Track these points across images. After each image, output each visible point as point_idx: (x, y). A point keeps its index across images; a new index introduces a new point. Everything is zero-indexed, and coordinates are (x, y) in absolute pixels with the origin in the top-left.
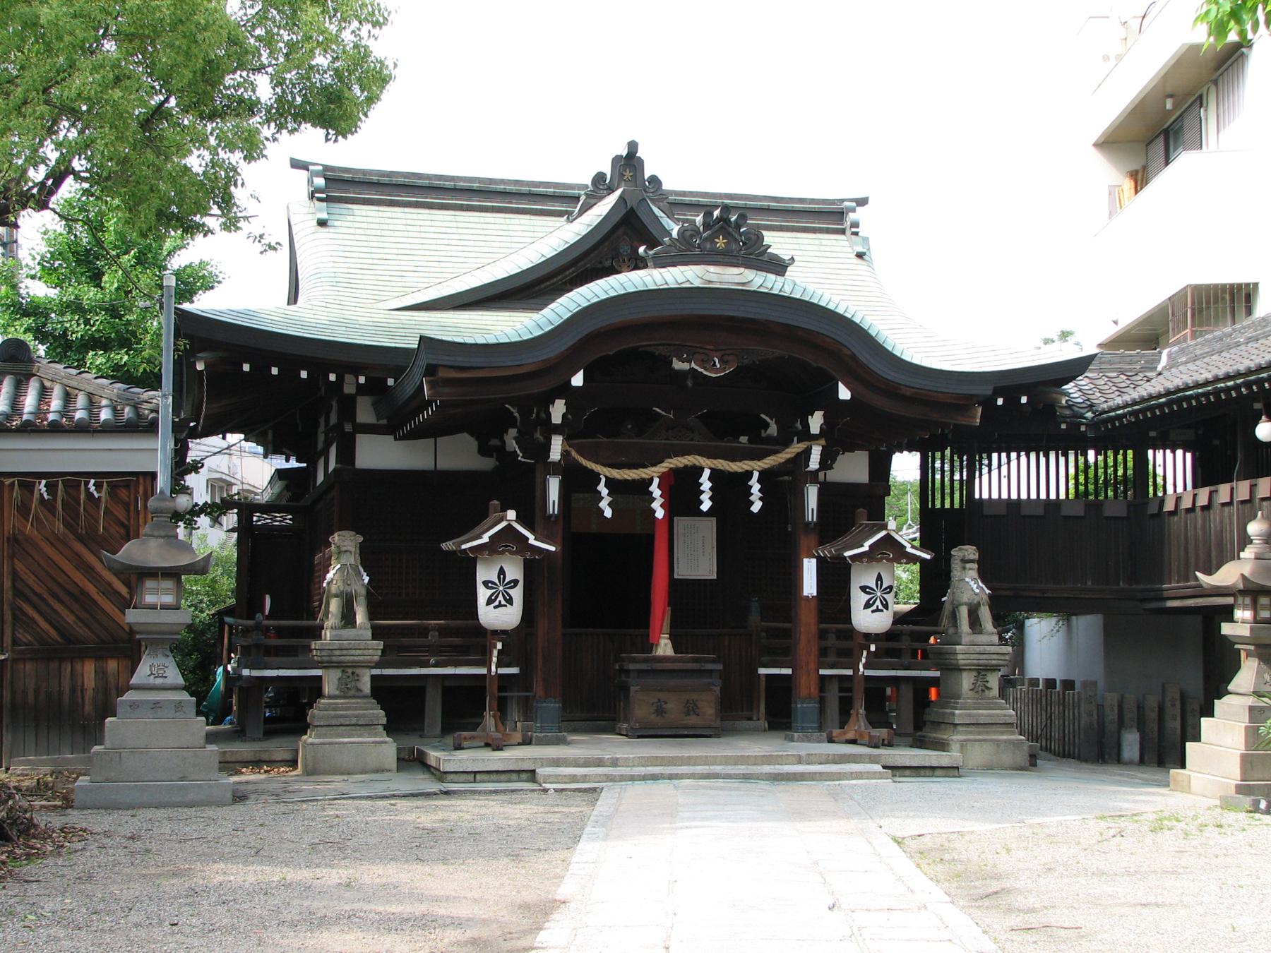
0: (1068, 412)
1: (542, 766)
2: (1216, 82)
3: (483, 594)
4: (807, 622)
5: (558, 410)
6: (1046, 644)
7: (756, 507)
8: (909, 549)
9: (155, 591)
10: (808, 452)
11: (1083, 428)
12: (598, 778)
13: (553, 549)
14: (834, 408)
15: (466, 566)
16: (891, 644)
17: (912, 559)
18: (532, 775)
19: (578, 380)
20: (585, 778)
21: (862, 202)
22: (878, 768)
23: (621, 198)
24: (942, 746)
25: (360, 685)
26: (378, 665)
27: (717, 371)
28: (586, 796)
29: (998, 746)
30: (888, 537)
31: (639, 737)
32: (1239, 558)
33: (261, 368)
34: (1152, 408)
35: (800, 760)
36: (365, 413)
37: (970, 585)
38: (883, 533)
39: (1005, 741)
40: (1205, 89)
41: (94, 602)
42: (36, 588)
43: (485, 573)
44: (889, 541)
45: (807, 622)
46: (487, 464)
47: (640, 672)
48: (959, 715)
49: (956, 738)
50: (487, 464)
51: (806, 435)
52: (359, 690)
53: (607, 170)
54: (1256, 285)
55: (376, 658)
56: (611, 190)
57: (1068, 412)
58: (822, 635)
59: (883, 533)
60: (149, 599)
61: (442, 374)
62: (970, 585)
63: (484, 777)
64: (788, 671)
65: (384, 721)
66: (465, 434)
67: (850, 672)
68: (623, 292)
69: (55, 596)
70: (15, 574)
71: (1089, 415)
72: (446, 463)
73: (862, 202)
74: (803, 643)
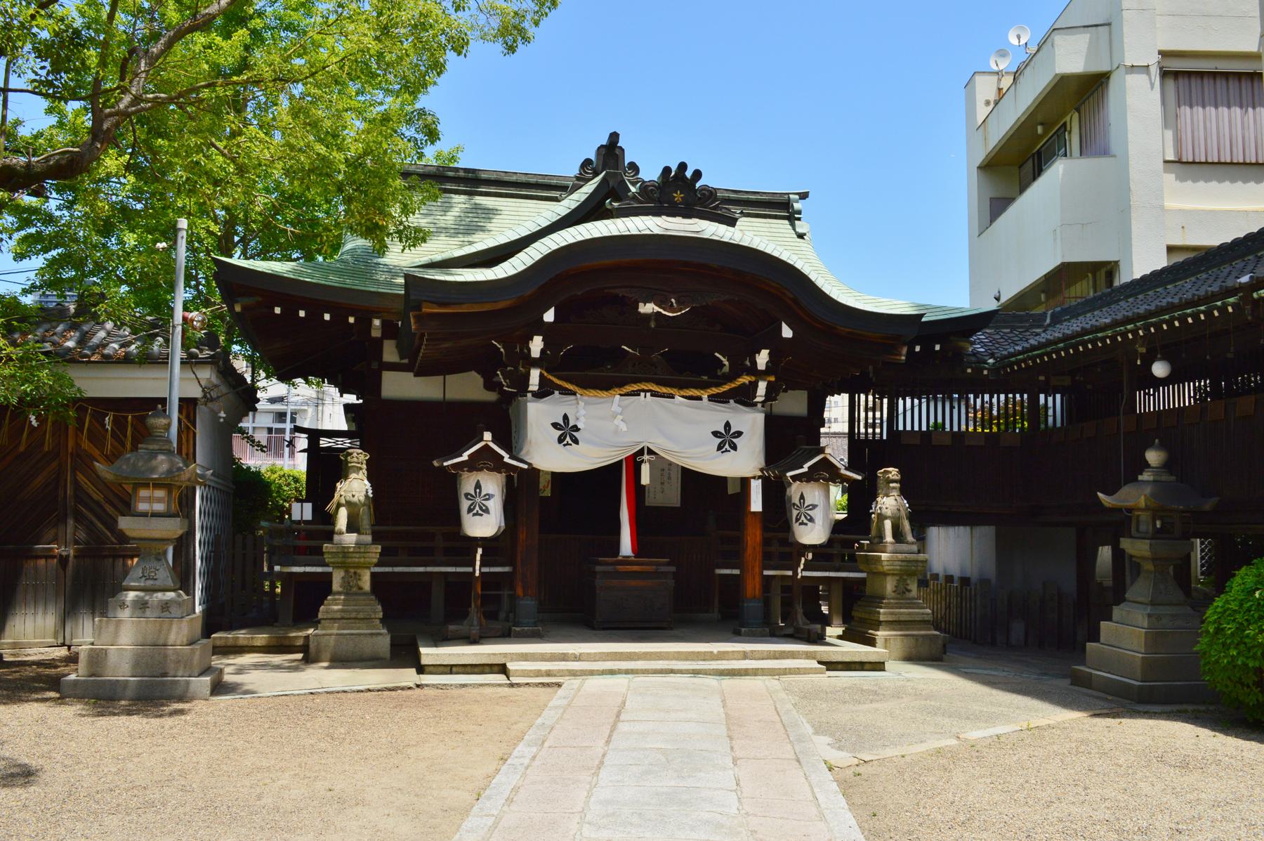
0: (973, 359)
3: (465, 504)
4: (753, 536)
5: (536, 345)
6: (950, 549)
7: (1100, 494)
8: (843, 471)
9: (149, 500)
10: (754, 386)
11: (985, 372)
12: (561, 673)
13: (859, 478)
14: (779, 349)
15: (450, 481)
16: (822, 555)
17: (843, 479)
18: (503, 669)
19: (549, 316)
20: (549, 674)
21: (804, 196)
22: (813, 664)
23: (604, 178)
24: (871, 642)
25: (360, 583)
26: (377, 565)
28: (1245, 84)
30: (825, 459)
31: (604, 629)
32: (1136, 480)
33: (290, 312)
34: (1033, 358)
35: (745, 656)
36: (390, 353)
37: (889, 503)
38: (821, 457)
39: (922, 636)
40: (1068, 119)
42: (95, 496)
43: (468, 483)
44: (826, 465)
45: (753, 536)
46: (491, 396)
47: (604, 573)
48: (883, 613)
49: (881, 634)
50: (491, 396)
51: (753, 370)
52: (360, 588)
53: (593, 157)
54: (1117, 263)
55: (375, 561)
56: (596, 174)
57: (973, 359)
58: (766, 542)
59: (821, 457)
60: (142, 507)
61: (426, 309)
62: (889, 503)
63: (460, 669)
64: (737, 572)
65: (381, 615)
66: (474, 373)
67: (790, 573)
68: (589, 237)
69: (112, 504)
70: (76, 484)
71: (991, 361)
72: (452, 395)
73: (804, 196)
74: (749, 551)
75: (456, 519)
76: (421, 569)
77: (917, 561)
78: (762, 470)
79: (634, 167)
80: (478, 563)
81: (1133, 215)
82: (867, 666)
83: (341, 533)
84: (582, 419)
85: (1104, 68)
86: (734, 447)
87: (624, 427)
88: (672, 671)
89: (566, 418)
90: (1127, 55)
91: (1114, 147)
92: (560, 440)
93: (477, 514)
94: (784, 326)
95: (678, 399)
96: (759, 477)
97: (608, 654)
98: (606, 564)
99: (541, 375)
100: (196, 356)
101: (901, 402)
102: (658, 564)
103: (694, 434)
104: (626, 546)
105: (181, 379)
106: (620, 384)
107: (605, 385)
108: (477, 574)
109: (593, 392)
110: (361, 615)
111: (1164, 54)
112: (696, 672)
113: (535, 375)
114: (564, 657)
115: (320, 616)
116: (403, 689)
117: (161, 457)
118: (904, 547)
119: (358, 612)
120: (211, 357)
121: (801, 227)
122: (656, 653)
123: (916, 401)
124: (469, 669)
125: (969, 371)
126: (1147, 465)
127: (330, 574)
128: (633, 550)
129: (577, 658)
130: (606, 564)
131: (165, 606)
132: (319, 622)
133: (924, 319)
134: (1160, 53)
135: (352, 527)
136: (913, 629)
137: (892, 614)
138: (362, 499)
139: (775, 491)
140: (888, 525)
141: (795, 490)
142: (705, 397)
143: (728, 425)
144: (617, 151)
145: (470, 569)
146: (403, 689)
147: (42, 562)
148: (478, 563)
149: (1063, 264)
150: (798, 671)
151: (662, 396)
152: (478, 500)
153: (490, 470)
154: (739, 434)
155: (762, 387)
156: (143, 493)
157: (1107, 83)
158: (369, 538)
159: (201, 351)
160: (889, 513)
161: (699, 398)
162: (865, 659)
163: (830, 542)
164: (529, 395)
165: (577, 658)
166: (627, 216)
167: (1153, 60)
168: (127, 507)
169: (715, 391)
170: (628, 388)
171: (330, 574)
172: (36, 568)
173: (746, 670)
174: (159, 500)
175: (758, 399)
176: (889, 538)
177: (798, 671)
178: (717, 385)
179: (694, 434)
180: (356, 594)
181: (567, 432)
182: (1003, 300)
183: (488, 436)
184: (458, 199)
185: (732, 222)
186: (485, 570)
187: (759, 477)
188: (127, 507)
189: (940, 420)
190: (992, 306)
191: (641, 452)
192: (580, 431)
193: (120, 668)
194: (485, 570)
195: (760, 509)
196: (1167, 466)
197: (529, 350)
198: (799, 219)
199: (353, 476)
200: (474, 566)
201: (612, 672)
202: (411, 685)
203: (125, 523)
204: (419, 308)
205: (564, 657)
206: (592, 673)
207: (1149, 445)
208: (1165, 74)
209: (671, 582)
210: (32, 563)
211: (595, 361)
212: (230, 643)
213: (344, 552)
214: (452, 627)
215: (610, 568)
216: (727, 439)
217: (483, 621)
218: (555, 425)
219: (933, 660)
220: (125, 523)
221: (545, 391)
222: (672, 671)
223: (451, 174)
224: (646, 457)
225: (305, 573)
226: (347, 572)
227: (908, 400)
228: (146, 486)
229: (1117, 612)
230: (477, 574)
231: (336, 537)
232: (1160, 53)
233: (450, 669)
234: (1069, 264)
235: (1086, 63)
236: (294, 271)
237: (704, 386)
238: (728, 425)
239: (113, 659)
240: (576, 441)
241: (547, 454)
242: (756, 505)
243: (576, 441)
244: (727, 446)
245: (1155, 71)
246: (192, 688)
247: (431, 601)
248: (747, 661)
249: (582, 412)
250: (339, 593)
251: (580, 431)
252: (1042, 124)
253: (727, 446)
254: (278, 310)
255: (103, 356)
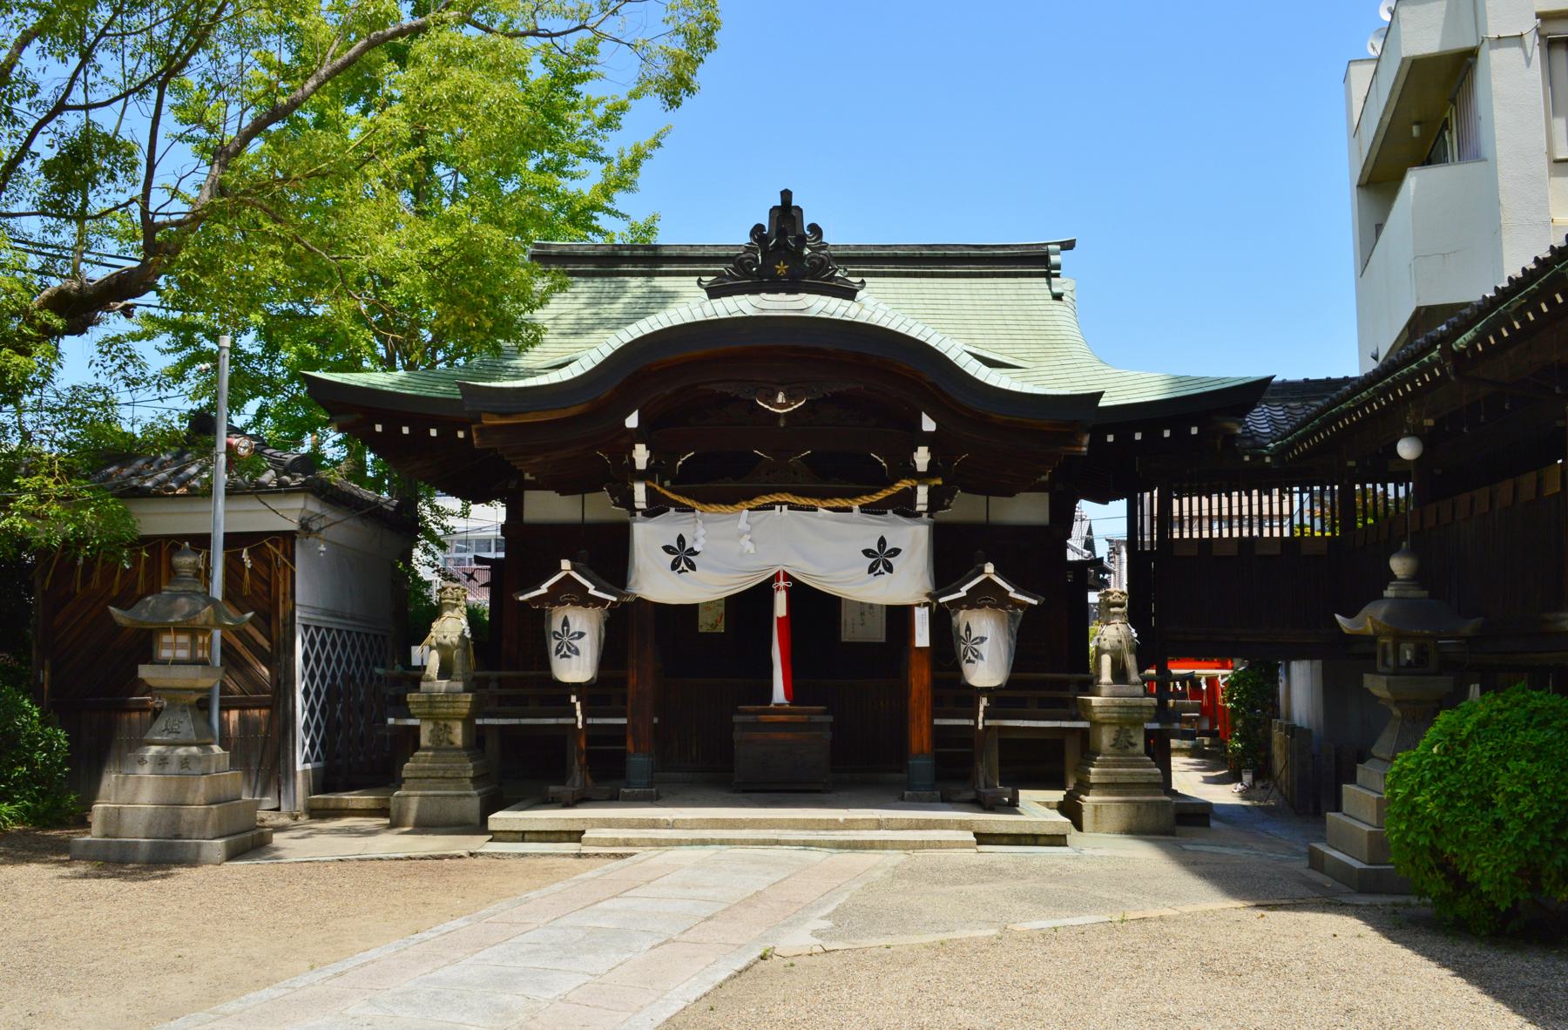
1: (592, 827)
2: (1453, 101)
4: (920, 678)
7: (1338, 617)
10: (913, 492)
11: (1268, 460)
13: (1035, 602)
20: (615, 842)
21: (1068, 245)
25: (452, 738)
27: (781, 406)
29: (1139, 808)
32: (1382, 597)
35: (879, 825)
39: (1147, 803)
41: (242, 657)
45: (920, 678)
53: (765, 222)
57: (1249, 443)
58: (936, 683)
60: (166, 654)
63: (534, 837)
73: (1068, 245)
74: (914, 695)
75: (547, 665)
76: (552, 721)
77: (1141, 707)
78: (928, 595)
79: (815, 229)
80: (981, 715)
81: (1505, 237)
82: (1042, 840)
83: (430, 680)
84: (702, 541)
85: (1468, 43)
86: (889, 569)
87: (750, 547)
88: (777, 842)
89: (681, 539)
90: (1490, 23)
91: (1485, 151)
92: (674, 566)
93: (565, 656)
94: (925, 417)
95: (822, 511)
96: (926, 604)
97: (708, 821)
98: (747, 713)
99: (648, 489)
100: (286, 484)
101: (1176, 503)
102: (811, 713)
103: (856, 556)
104: (779, 694)
105: (226, 512)
106: (749, 497)
107: (729, 498)
108: (980, 726)
109: (715, 508)
110: (449, 774)
111: (1544, 17)
112: (807, 844)
113: (640, 491)
114: (655, 824)
115: (404, 774)
116: (451, 857)
117: (183, 600)
118: (1124, 688)
119: (445, 770)
120: (303, 484)
121: (1058, 285)
122: (766, 820)
123: (1225, 500)
124: (543, 837)
125: (1247, 458)
126: (1391, 576)
127: (417, 728)
128: (787, 696)
129: (670, 825)
130: (747, 713)
131: (185, 762)
132: (403, 780)
133: (1102, 404)
134: (1538, 15)
135: (445, 672)
136: (1136, 794)
137: (1107, 774)
138: (456, 640)
139: (942, 621)
140: (1106, 660)
141: (963, 617)
142: (856, 507)
143: (882, 541)
144: (794, 213)
145: (572, 721)
146: (451, 857)
147: (136, 715)
148: (981, 715)
149: (1419, 309)
150: (939, 845)
151: (801, 508)
152: (566, 639)
153: (574, 604)
154: (896, 552)
155: (922, 494)
156: (167, 639)
157: (1475, 62)
158: (459, 686)
159: (293, 478)
160: (1107, 646)
161: (849, 510)
162: (1038, 832)
163: (1011, 683)
164: (639, 514)
165: (670, 825)
166: (730, 295)
167: (1528, 25)
168: (149, 657)
169: (867, 500)
170: (759, 501)
171: (417, 728)
172: (130, 721)
173: (872, 842)
174: (183, 646)
175: (919, 508)
176: (1106, 676)
177: (939, 845)
178: (870, 493)
179: (856, 556)
180: (446, 749)
181: (682, 556)
182: (1381, 358)
183: (566, 564)
184: (635, 283)
185: (849, 294)
186: (988, 723)
187: (926, 604)
188: (149, 657)
189: (1265, 499)
190: (1373, 365)
191: (776, 577)
192: (701, 557)
193: (136, 833)
194: (988, 723)
195: (927, 644)
196: (1418, 577)
197: (633, 461)
198: (1057, 276)
199: (447, 614)
200: (975, 716)
201: (704, 842)
202: (463, 853)
203: (144, 671)
204: (479, 420)
205: (655, 824)
206: (679, 843)
207: (1394, 550)
208: (1551, 44)
209: (828, 735)
210: (125, 717)
211: (720, 472)
212: (331, 805)
213: (432, 700)
214: (552, 788)
215: (750, 718)
216: (881, 558)
217: (589, 781)
218: (667, 549)
219: (1154, 833)
220: (144, 671)
221: (656, 507)
222: (777, 842)
223: (627, 253)
224: (782, 583)
225: (520, 725)
226: (436, 724)
227: (1195, 500)
228: (167, 631)
229: (1362, 771)
230: (980, 726)
231: (423, 685)
232: (1538, 15)
233: (523, 836)
234: (1429, 308)
235: (1442, 44)
236: (402, 383)
237: (853, 495)
238: (882, 541)
239: (127, 820)
240: (692, 567)
241: (655, 581)
242: (922, 638)
243: (692, 567)
244: (881, 567)
245: (1532, 41)
246: (205, 852)
247: (541, 757)
248: (882, 832)
249: (701, 531)
250: (427, 749)
251: (701, 557)
252: (1418, 123)
253: (881, 567)
254: (379, 428)
255: (190, 489)
